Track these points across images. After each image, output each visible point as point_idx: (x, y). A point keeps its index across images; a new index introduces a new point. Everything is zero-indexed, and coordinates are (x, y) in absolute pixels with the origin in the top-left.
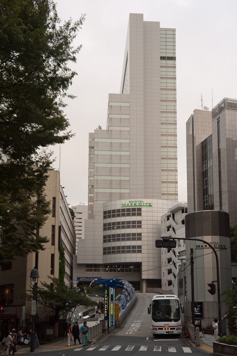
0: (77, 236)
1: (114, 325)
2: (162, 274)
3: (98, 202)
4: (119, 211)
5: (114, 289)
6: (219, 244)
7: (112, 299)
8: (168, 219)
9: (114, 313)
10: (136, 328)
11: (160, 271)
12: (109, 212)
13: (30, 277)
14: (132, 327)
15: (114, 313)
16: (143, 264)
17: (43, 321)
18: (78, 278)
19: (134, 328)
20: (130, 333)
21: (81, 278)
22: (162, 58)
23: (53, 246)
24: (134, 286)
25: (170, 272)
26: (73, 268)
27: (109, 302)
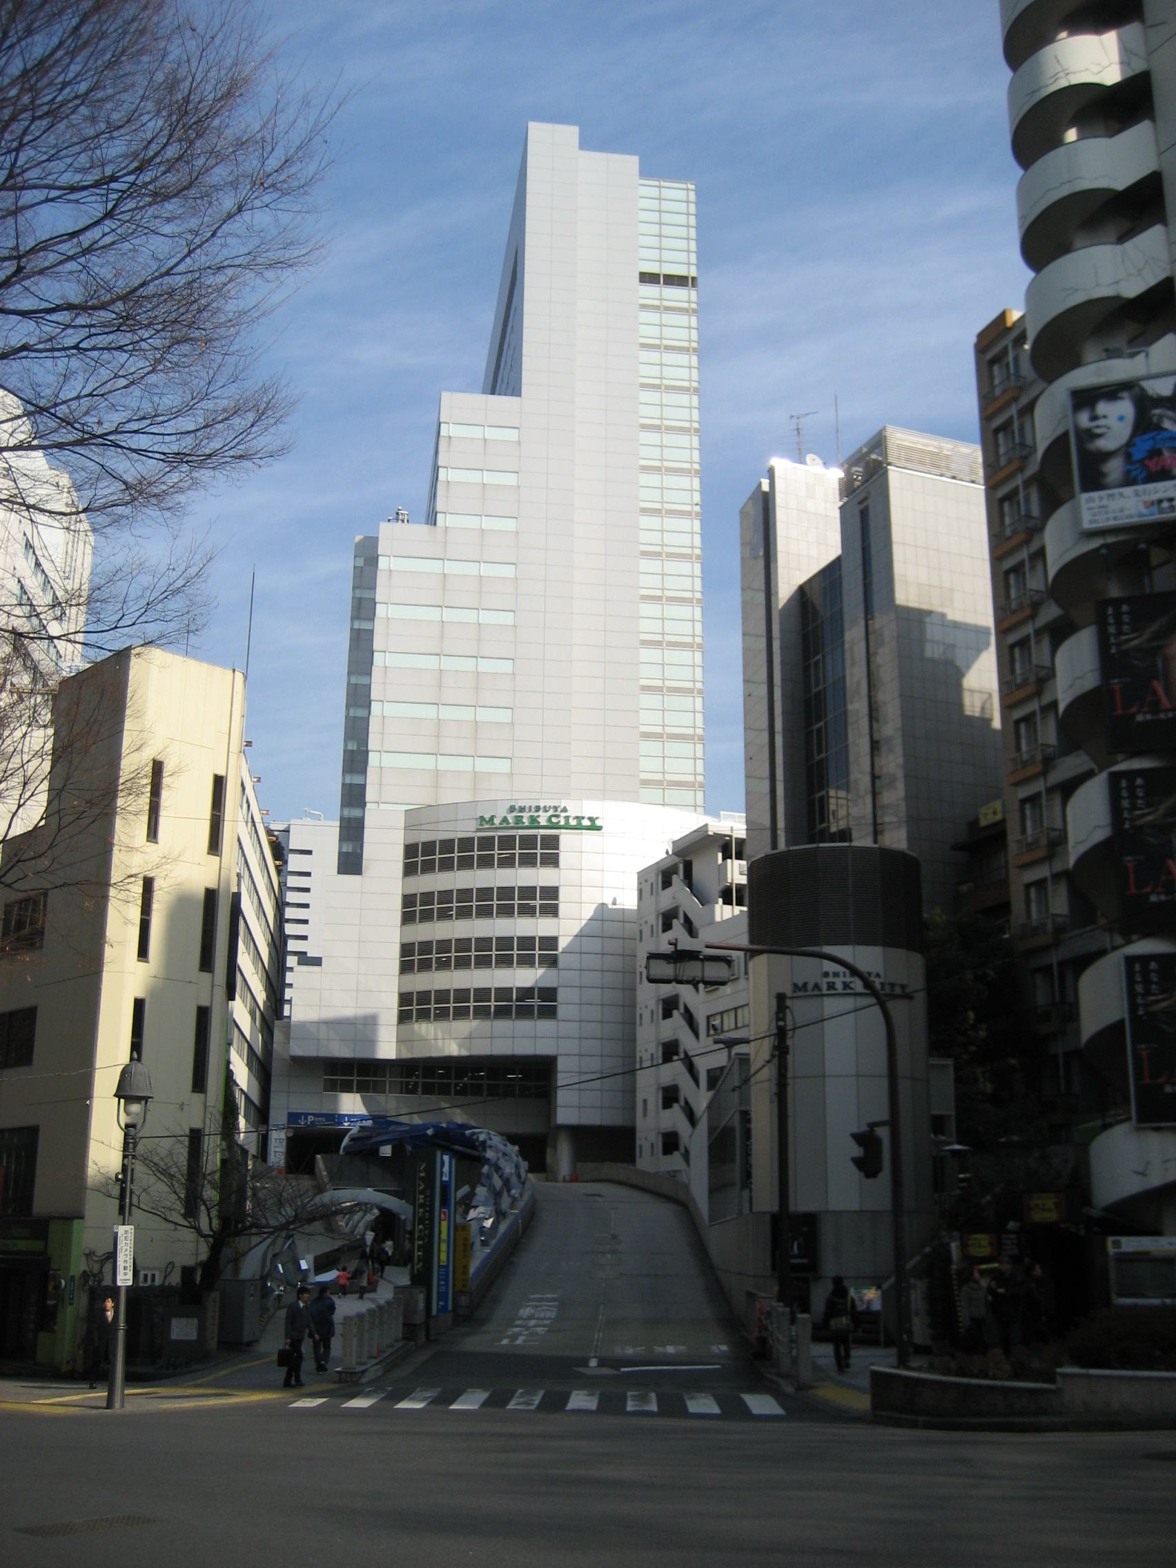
0: (292, 945)
1: (450, 1308)
2: (639, 1105)
3: (382, 806)
4: (466, 844)
5: (454, 1161)
6: (882, 980)
7: (445, 1202)
8: (667, 883)
9: (451, 1259)
10: (540, 1322)
11: (630, 1091)
12: (429, 847)
13: (115, 1095)
14: (521, 1319)
15: (451, 1259)
16: (562, 1064)
17: (157, 1282)
18: (293, 1117)
19: (532, 1323)
20: (519, 1341)
21: (306, 1115)
22: (648, 278)
23: (207, 976)
24: (523, 1153)
25: (670, 1096)
26: (273, 1073)
27: (432, 1212)
